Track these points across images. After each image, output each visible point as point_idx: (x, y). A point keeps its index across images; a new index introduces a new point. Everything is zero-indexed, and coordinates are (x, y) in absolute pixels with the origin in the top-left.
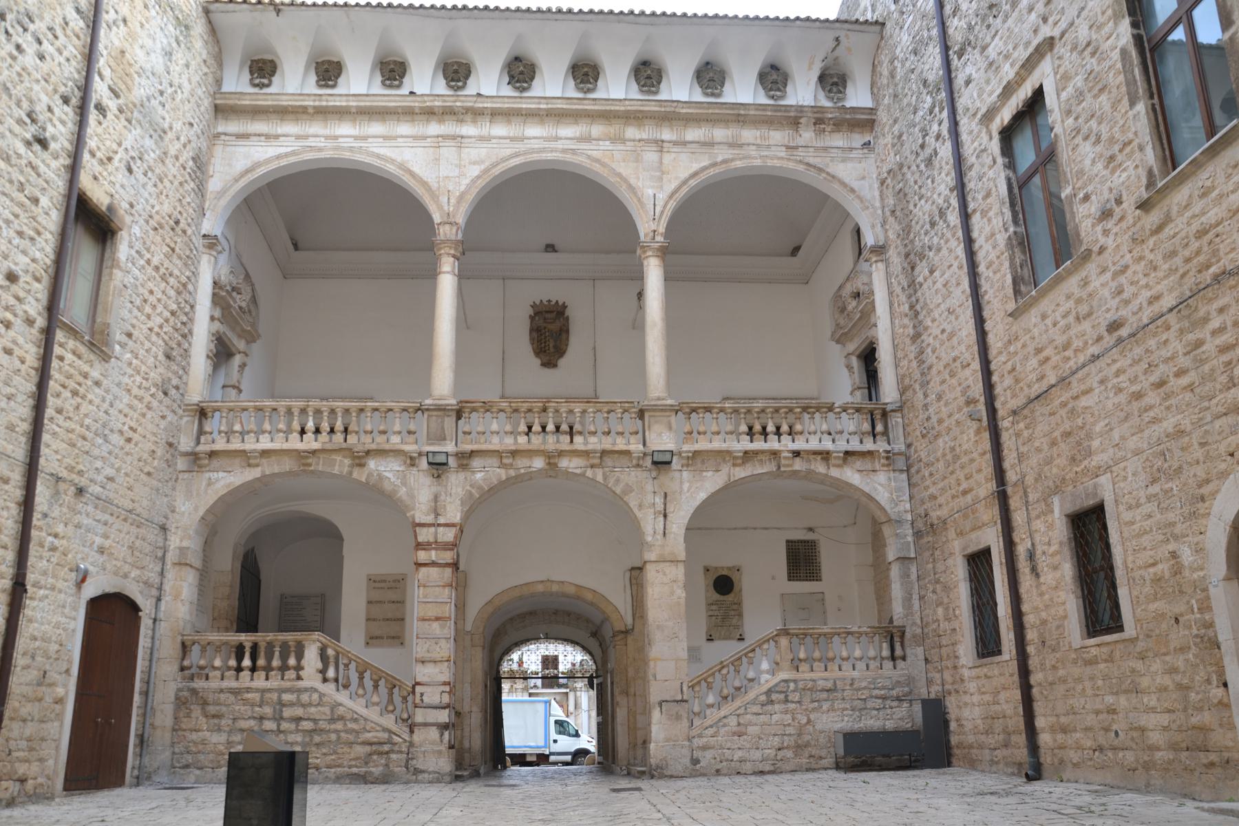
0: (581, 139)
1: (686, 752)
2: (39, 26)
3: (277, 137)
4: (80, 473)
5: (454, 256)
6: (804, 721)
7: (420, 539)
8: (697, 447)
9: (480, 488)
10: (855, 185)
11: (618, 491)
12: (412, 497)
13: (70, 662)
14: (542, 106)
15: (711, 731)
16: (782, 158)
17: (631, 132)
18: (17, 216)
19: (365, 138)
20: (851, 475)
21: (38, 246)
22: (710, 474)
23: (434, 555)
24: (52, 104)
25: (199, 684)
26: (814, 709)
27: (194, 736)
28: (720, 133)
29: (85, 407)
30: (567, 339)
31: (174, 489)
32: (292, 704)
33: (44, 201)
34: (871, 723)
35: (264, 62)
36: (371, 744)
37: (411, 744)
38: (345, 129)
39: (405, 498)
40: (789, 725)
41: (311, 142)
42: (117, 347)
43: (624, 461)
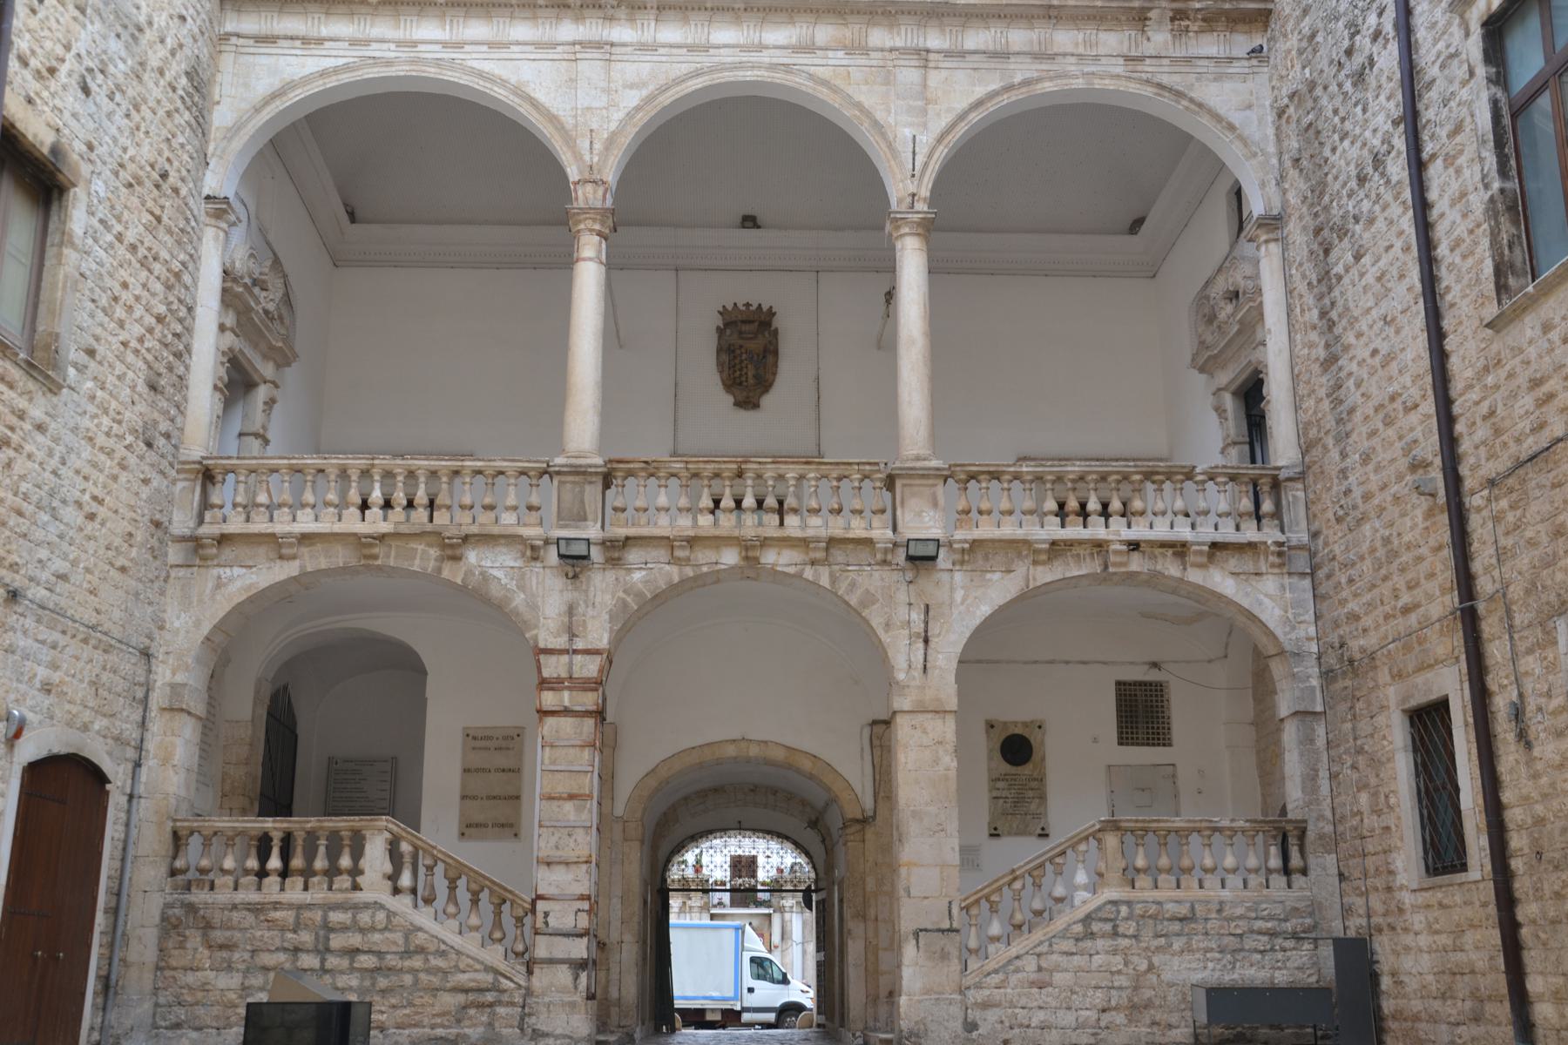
1: (956, 1010)
3: (320, 41)
5: (599, 234)
6: (1144, 966)
7: (546, 673)
8: (977, 534)
9: (639, 594)
10: (1236, 118)
11: (853, 601)
12: (534, 607)
15: (995, 979)
16: (1118, 76)
19: (459, 45)
20: (1221, 581)
22: (996, 576)
23: (566, 698)
25: (199, 896)
26: (1159, 949)
28: (1019, 37)
30: (776, 365)
31: (162, 593)
32: (344, 928)
34: (1252, 973)
36: (466, 991)
37: (529, 992)
39: (522, 609)
40: (1119, 972)
41: (375, 51)
42: (72, 371)
43: (864, 554)
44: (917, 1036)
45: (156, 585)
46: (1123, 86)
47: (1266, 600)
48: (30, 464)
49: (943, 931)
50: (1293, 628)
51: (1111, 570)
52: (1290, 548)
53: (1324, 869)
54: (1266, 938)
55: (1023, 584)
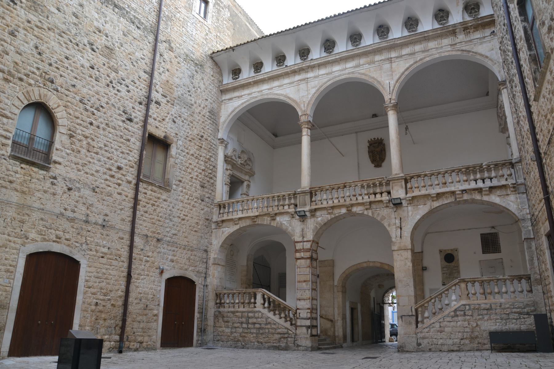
0: (355, 67)
1: (414, 340)
2: (128, 81)
3: (241, 96)
4: (158, 233)
5: (307, 128)
6: (475, 325)
7: (297, 248)
8: (414, 194)
9: (320, 224)
10: (488, 54)
11: (379, 219)
12: (294, 230)
13: (159, 301)
14: (337, 57)
15: (426, 330)
16: (449, 51)
17: (378, 58)
18: (120, 147)
19: (271, 89)
20: (495, 198)
21: (131, 155)
22: (422, 206)
23: (302, 254)
24: (134, 106)
25: (221, 309)
26: (479, 319)
27: (220, 329)
28: (418, 48)
29: (158, 210)
30: (385, 153)
31: (211, 236)
32: (252, 318)
33: (133, 140)
34: (513, 326)
35: (236, 69)
36: (281, 334)
37: (296, 334)
38: (265, 86)
39: (291, 231)
40: (467, 327)
41: (254, 95)
42: (174, 186)
43: (381, 205)
44: (403, 347)
45: (208, 234)
46: (450, 53)
47: (511, 203)
48: (162, 209)
49: (410, 316)
50: (521, 211)
51: (458, 200)
52: (518, 185)
53: (538, 290)
54: (517, 315)
55: (429, 208)
